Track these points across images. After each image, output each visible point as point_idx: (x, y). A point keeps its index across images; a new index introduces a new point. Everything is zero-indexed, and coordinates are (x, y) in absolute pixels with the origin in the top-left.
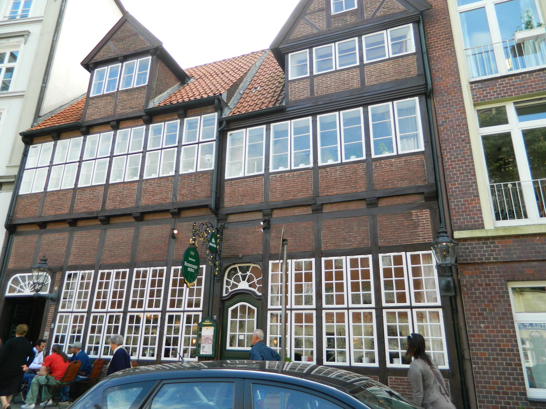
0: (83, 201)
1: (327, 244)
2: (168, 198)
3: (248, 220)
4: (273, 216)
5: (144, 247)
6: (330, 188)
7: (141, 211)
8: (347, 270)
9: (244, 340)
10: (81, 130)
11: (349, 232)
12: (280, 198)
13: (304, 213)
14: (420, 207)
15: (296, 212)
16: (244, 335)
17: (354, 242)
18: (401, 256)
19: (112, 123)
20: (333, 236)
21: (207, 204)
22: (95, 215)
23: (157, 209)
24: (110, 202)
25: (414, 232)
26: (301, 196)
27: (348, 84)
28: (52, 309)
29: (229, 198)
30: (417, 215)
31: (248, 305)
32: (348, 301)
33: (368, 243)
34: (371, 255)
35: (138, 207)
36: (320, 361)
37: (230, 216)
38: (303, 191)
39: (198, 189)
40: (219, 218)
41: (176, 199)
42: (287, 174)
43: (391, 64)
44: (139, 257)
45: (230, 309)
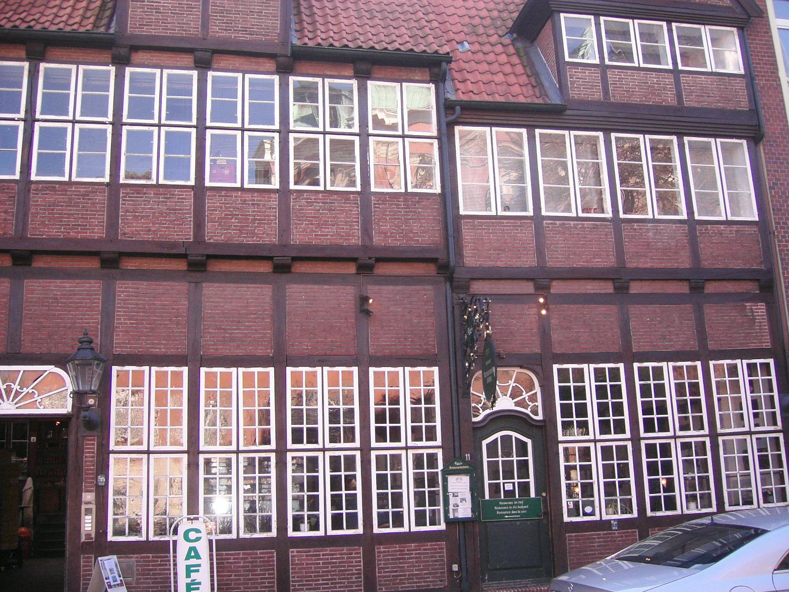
0: (142, 217)
1: (639, 342)
2: (354, 236)
3: (508, 293)
4: (552, 291)
5: (302, 326)
6: (641, 256)
7: (294, 254)
8: (590, 384)
9: (666, 478)
10: (114, 50)
11: (668, 326)
12: (564, 262)
13: (602, 292)
14: (754, 299)
15: (589, 287)
16: (514, 483)
17: (677, 342)
18: (661, 368)
19: (199, 54)
20: (647, 332)
21: (355, 256)
22: (182, 251)
23: (329, 253)
24: (212, 226)
25: (749, 333)
26: (599, 263)
27: (659, 95)
28: (90, 448)
29: (474, 250)
30: (752, 309)
31: (514, 435)
32: (749, 422)
33: (693, 345)
34: (700, 362)
35: (285, 246)
36: (721, 508)
37: (475, 283)
38: (601, 255)
39: (416, 226)
40: (454, 284)
41: (371, 239)
42: (572, 223)
43: (715, 82)
44: (293, 345)
45: (485, 443)
